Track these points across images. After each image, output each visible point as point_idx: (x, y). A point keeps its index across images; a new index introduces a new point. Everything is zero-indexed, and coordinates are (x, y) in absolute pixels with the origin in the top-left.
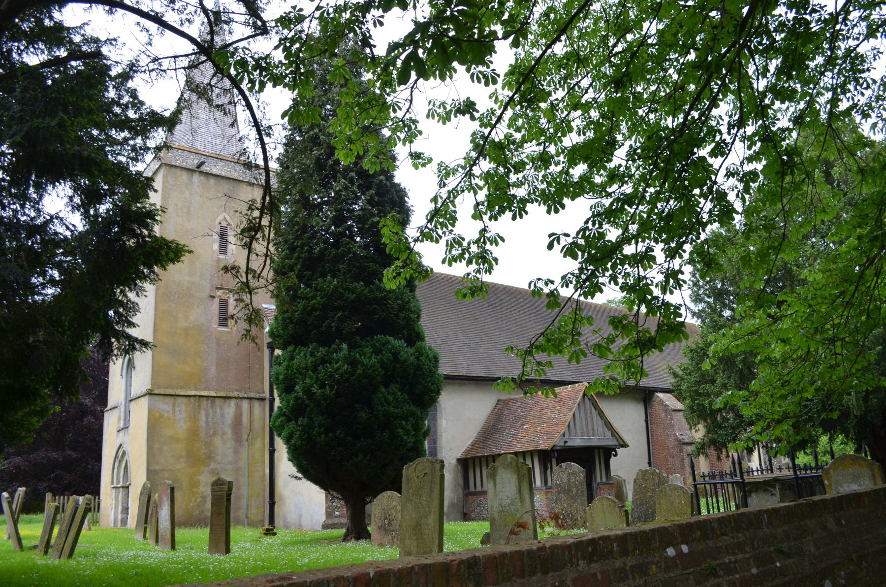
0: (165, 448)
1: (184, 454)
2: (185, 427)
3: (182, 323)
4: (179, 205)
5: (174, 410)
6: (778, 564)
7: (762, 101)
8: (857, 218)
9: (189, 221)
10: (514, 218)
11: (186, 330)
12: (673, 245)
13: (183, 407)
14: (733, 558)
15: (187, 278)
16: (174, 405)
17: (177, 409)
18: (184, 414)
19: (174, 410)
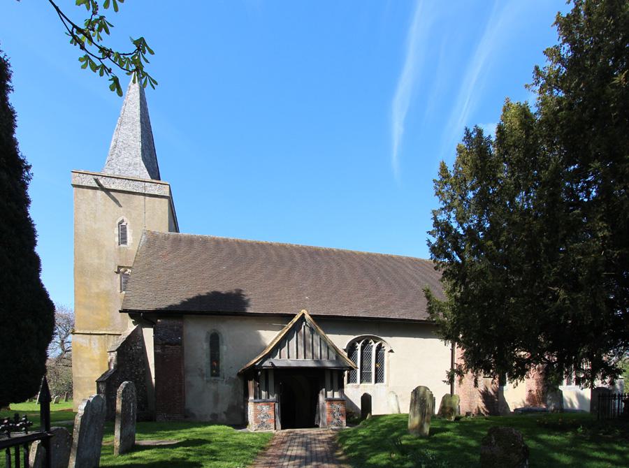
0: (85, 365)
1: (98, 368)
2: (99, 353)
3: (95, 290)
4: (87, 213)
5: (90, 342)
6: (570, 322)
7: (479, 351)
8: (325, 445)
9: (95, 223)
10: (434, 181)
11: (98, 295)
12: (533, 262)
13: (97, 341)
14: (412, 281)
15: (96, 261)
16: (90, 340)
17: (92, 342)
18: (97, 345)
19: (90, 342)
